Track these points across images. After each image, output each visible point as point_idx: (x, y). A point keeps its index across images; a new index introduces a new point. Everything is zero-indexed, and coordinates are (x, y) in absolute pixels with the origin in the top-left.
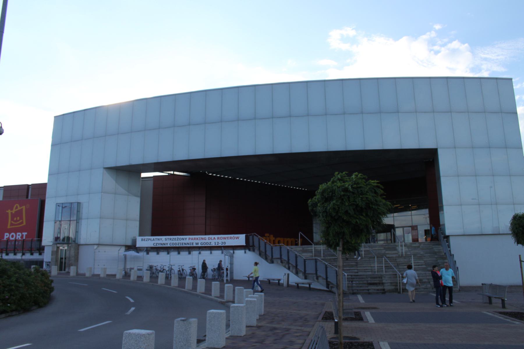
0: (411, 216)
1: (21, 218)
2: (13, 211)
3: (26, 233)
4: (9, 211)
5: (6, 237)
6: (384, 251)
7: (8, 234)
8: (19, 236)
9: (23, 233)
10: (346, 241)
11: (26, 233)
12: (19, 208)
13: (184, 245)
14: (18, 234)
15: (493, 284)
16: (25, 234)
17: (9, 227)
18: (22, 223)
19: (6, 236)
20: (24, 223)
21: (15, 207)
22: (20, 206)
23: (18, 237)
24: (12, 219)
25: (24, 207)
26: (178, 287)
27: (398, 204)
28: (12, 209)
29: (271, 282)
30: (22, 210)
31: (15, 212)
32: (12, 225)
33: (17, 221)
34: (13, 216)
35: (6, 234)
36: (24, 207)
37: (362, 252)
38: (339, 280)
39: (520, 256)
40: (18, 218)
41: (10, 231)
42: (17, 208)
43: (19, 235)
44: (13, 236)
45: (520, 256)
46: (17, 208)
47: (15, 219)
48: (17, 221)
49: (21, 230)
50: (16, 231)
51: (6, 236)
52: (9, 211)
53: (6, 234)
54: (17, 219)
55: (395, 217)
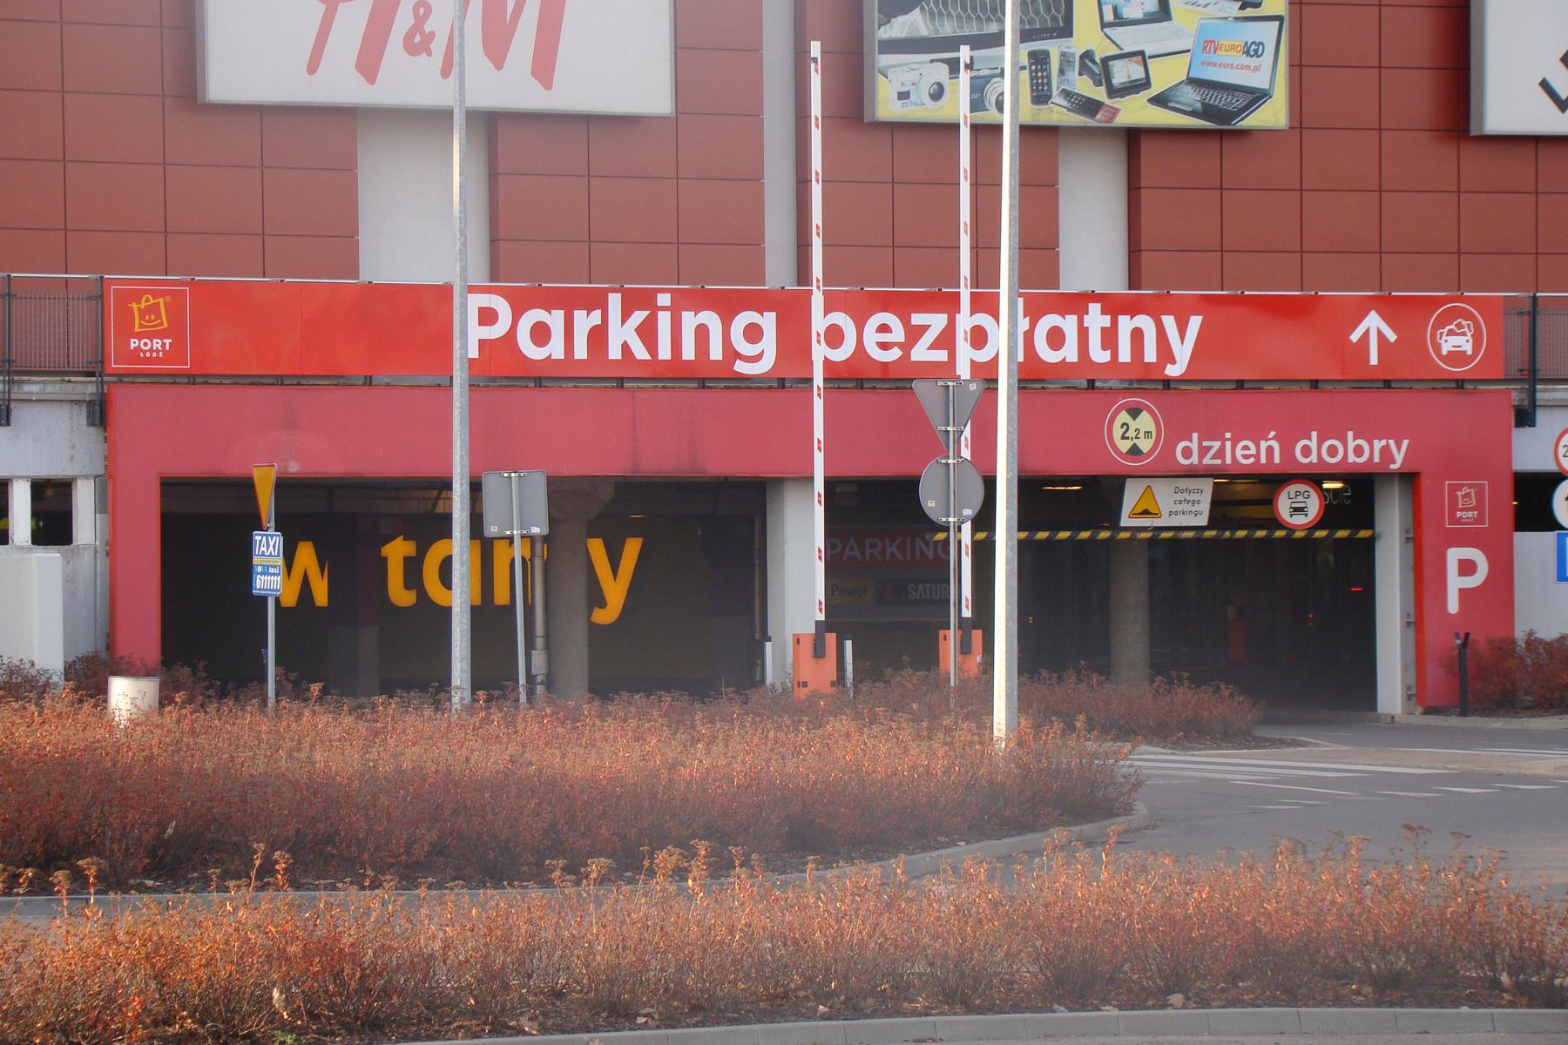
0: (1533, 197)
1: (159, 316)
2: (143, 305)
3: (170, 341)
4: (135, 306)
7: (136, 340)
8: (157, 344)
9: (164, 341)
11: (170, 341)
12: (1468, 491)
14: (155, 341)
16: (167, 341)
17: (137, 329)
18: (161, 324)
19: (134, 343)
20: (1474, 504)
21: (144, 298)
24: (1463, 500)
25: (161, 301)
28: (139, 302)
31: (145, 306)
32: (141, 326)
33: (150, 321)
34: (1463, 497)
35: (132, 340)
36: (161, 301)
39: (1545, 85)
40: (153, 317)
41: (1462, 510)
42: (147, 300)
43: (157, 343)
45: (1545, 85)
46: (147, 300)
47: (147, 318)
48: (150, 321)
49: (161, 335)
50: (151, 336)
51: (134, 343)
52: (135, 306)
53: (132, 340)
54: (150, 317)
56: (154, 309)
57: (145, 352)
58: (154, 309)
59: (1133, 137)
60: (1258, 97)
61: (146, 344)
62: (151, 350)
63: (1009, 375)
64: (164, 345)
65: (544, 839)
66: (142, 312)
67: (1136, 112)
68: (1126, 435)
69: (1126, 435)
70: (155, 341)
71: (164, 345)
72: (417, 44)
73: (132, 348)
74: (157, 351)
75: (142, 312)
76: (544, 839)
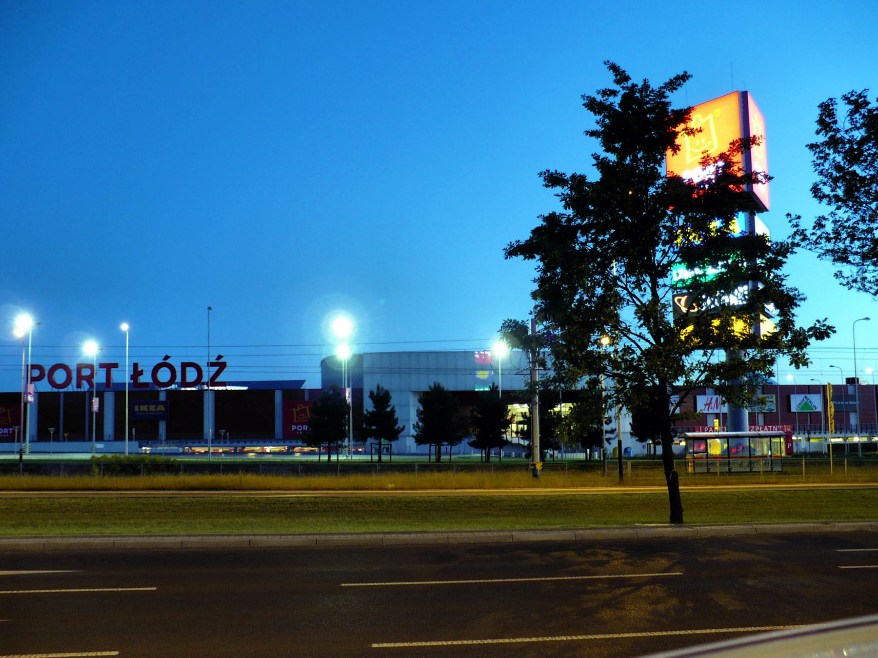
4: (294, 410)
5: (293, 429)
6: (762, 177)
10: (759, 468)
12: (303, 407)
13: (750, 430)
14: (304, 426)
15: (337, 357)
17: (295, 421)
18: (8, 421)
19: (294, 428)
22: (304, 406)
23: (304, 429)
24: (298, 415)
25: (307, 407)
26: (856, 412)
27: (115, 650)
28: (296, 408)
29: (478, 453)
30: (305, 409)
32: (297, 419)
35: (293, 426)
37: (857, 451)
38: (111, 533)
42: (300, 407)
44: (300, 428)
48: (302, 417)
51: (294, 428)
52: (294, 410)
53: (293, 426)
55: (851, 348)
56: (304, 411)
57: (299, 431)
58: (304, 411)
59: (764, 413)
60: (773, 410)
61: (300, 428)
62: (302, 431)
63: (573, 485)
64: (9, 431)
65: (870, 282)
66: (298, 413)
67: (764, 411)
68: (216, 369)
69: (216, 369)
70: (304, 426)
71: (9, 431)
72: (711, 408)
73: (49, 429)
74: (6, 434)
75: (298, 413)
76: (870, 282)
